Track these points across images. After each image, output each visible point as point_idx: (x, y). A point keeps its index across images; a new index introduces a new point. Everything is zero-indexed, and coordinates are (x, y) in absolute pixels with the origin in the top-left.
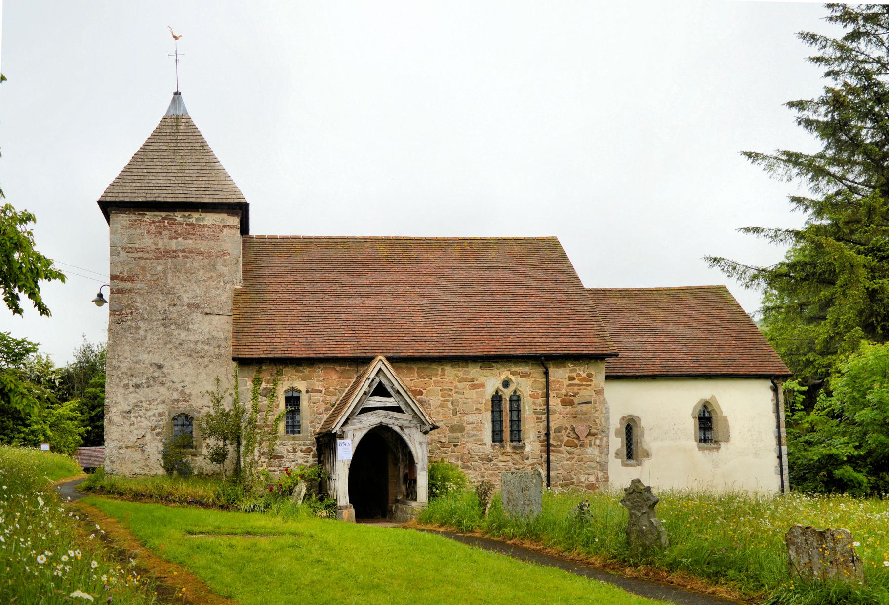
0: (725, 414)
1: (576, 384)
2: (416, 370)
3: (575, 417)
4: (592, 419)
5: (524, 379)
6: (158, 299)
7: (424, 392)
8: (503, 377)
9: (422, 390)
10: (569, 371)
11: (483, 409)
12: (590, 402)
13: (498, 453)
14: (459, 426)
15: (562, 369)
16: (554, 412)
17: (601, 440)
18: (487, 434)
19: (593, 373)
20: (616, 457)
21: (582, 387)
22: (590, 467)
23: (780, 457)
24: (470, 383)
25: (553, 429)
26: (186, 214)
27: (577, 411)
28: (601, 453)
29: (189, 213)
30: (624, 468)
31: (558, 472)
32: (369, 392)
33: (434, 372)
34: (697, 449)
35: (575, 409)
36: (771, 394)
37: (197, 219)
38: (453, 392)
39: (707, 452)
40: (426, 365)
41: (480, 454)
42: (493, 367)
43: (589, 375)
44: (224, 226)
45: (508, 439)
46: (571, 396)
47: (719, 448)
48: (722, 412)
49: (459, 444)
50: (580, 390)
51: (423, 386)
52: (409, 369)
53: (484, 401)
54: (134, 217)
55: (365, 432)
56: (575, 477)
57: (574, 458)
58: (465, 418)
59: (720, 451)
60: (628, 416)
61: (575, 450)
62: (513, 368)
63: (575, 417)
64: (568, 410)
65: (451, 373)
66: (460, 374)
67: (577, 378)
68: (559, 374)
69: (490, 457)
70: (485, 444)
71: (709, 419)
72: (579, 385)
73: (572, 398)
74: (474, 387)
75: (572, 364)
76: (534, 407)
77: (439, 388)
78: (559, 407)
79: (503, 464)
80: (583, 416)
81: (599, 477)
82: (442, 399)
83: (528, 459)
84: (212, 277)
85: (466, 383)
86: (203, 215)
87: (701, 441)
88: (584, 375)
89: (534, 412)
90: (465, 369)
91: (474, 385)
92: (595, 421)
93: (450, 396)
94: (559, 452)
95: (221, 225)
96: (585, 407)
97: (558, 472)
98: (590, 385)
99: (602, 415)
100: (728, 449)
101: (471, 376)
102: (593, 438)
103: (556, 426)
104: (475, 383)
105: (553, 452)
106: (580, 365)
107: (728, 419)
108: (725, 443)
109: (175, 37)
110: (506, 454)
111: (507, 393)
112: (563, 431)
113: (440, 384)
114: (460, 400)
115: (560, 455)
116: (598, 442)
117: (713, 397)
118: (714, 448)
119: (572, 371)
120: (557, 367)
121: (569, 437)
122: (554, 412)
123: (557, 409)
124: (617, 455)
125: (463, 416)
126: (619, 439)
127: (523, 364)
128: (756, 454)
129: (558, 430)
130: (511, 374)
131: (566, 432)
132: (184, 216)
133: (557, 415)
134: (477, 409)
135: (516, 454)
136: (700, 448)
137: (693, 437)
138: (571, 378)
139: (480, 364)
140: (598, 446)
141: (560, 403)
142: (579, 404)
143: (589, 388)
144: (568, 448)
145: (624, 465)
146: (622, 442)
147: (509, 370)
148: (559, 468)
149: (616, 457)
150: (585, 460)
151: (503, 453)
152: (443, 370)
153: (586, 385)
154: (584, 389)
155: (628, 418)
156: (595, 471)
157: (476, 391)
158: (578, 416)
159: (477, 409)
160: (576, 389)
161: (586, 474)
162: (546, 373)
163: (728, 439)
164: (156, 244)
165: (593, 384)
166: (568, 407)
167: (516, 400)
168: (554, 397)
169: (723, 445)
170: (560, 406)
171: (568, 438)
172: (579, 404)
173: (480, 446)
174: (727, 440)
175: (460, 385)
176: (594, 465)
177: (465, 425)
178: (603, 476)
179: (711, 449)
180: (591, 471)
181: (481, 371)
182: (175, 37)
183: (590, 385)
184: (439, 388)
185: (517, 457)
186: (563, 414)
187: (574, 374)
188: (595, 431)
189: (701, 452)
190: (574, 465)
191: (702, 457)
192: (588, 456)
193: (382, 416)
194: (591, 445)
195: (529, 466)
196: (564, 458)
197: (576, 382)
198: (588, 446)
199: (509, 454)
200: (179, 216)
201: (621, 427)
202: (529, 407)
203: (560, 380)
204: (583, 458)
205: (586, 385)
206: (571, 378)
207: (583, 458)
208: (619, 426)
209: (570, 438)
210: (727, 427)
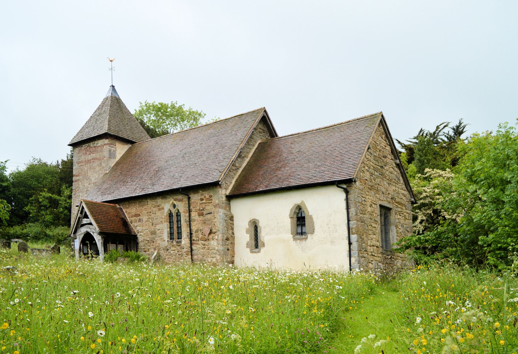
0: (310, 214)
1: (204, 203)
2: (138, 203)
3: (205, 223)
4: (213, 223)
5: (180, 202)
6: (85, 182)
7: (141, 214)
8: (171, 202)
9: (140, 213)
10: (200, 195)
11: (163, 222)
12: (211, 213)
13: (170, 246)
14: (154, 231)
15: (197, 194)
16: (194, 220)
17: (218, 235)
18: (166, 236)
19: (212, 195)
20: (247, 247)
21: (207, 204)
22: (213, 253)
23: (350, 244)
24: (158, 208)
25: (194, 230)
26: (93, 142)
27: (205, 219)
28: (218, 244)
29: (89, 144)
30: (251, 254)
31: (198, 256)
32: (82, 216)
33: (144, 203)
34: (292, 239)
35: (204, 218)
36: (344, 195)
37: (96, 144)
38: (152, 213)
39: (298, 241)
40: (141, 201)
41: (163, 246)
42: (167, 197)
43: (211, 196)
44: (104, 145)
45: (177, 237)
46: (202, 210)
47: (307, 238)
48: (308, 212)
49: (155, 241)
50: (206, 206)
51: (140, 211)
52: (135, 203)
53: (164, 217)
54: (79, 148)
55: (82, 235)
56: (206, 259)
57: (205, 248)
58: (157, 227)
59: (307, 240)
60: (253, 220)
61: (206, 243)
62: (175, 197)
63: (205, 223)
64: (201, 218)
65: (150, 203)
66: (154, 203)
67: (204, 199)
68: (195, 198)
69: (168, 248)
70: (165, 241)
71: (303, 218)
72: (205, 203)
73: (203, 211)
74: (159, 210)
75: (201, 190)
76: (185, 218)
77: (146, 212)
78: (197, 217)
79: (173, 252)
80: (208, 222)
81: (218, 259)
82: (148, 217)
83: (183, 249)
84: (100, 169)
85: (156, 208)
86: (98, 141)
87: (298, 233)
88: (207, 197)
89: (185, 221)
90: (156, 200)
91: (160, 208)
92: (214, 225)
93: (150, 215)
94: (198, 244)
95: (103, 144)
96: (209, 216)
97: (198, 256)
98: (211, 202)
99: (218, 220)
100: (312, 239)
101: (159, 204)
102: (214, 235)
103: (196, 229)
104: (160, 207)
105: (195, 244)
106: (206, 190)
107: (313, 217)
108: (311, 235)
109: (111, 61)
110: (174, 246)
111: (174, 211)
112: (199, 231)
113: (146, 210)
114: (155, 217)
115: (198, 246)
116: (216, 237)
117: (303, 202)
118: (303, 239)
119: (202, 195)
120: (195, 194)
121: (202, 235)
122: (194, 220)
123: (196, 219)
124: (248, 245)
125: (156, 226)
126: (248, 235)
127: (179, 194)
128: (332, 242)
129: (197, 231)
130: (174, 200)
131: (201, 232)
132: (93, 144)
133: (196, 222)
134: (161, 222)
135: (179, 246)
136: (295, 239)
137: (290, 231)
138: (202, 200)
139: (161, 197)
140: (217, 240)
141: (197, 215)
142: (206, 214)
143: (211, 204)
144: (202, 242)
145: (252, 252)
146: (250, 237)
147: (173, 198)
148: (198, 254)
149: (247, 247)
150: (210, 249)
151: (173, 245)
152: (147, 202)
153: (209, 203)
154: (208, 205)
155: (253, 221)
156: (216, 255)
157: (161, 212)
158: (206, 222)
159: (161, 222)
160: (204, 205)
161: (211, 257)
162: (189, 198)
163: (314, 231)
164: (85, 158)
165: (212, 201)
166: (201, 217)
167: (178, 215)
168: (194, 211)
169: (309, 236)
170: (197, 217)
171: (202, 236)
172: (206, 214)
173: (163, 242)
174: (313, 232)
175: (154, 209)
176: (215, 251)
177: (156, 231)
178: (220, 258)
179: (301, 240)
180: (214, 256)
181: (162, 200)
182: (111, 61)
183: (211, 202)
184: (146, 212)
185: (179, 248)
186: (199, 221)
187: (203, 197)
188: (215, 231)
189: (294, 241)
190: (205, 252)
191: (295, 246)
192: (211, 246)
193: (87, 228)
194: (213, 239)
195: (184, 252)
196: (200, 248)
197: (204, 201)
198: (212, 240)
199: (175, 246)
200: (91, 144)
201: (249, 227)
202: (183, 218)
203: (196, 201)
204: (209, 248)
205: (209, 203)
206: (202, 200)
207: (209, 248)
208: (248, 227)
209: (203, 236)
210: (312, 223)
